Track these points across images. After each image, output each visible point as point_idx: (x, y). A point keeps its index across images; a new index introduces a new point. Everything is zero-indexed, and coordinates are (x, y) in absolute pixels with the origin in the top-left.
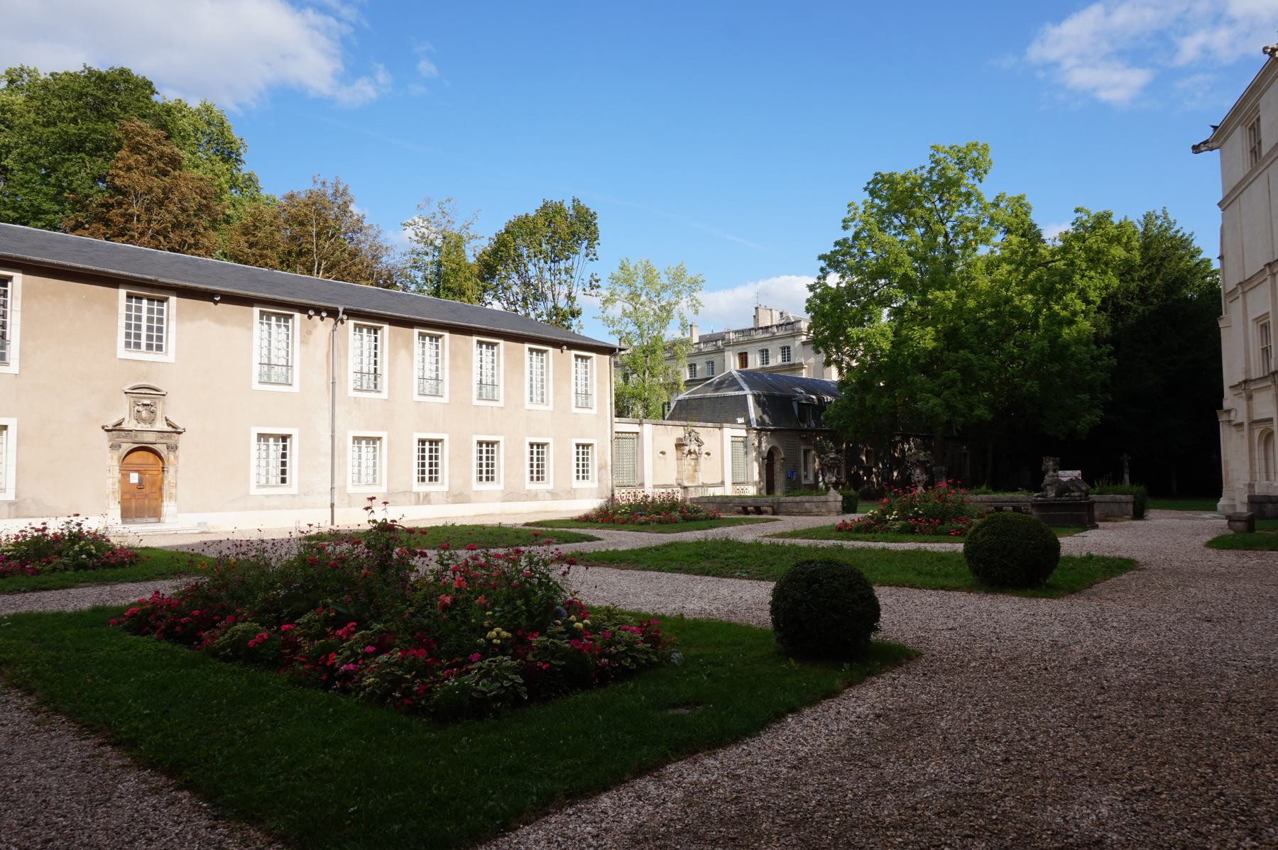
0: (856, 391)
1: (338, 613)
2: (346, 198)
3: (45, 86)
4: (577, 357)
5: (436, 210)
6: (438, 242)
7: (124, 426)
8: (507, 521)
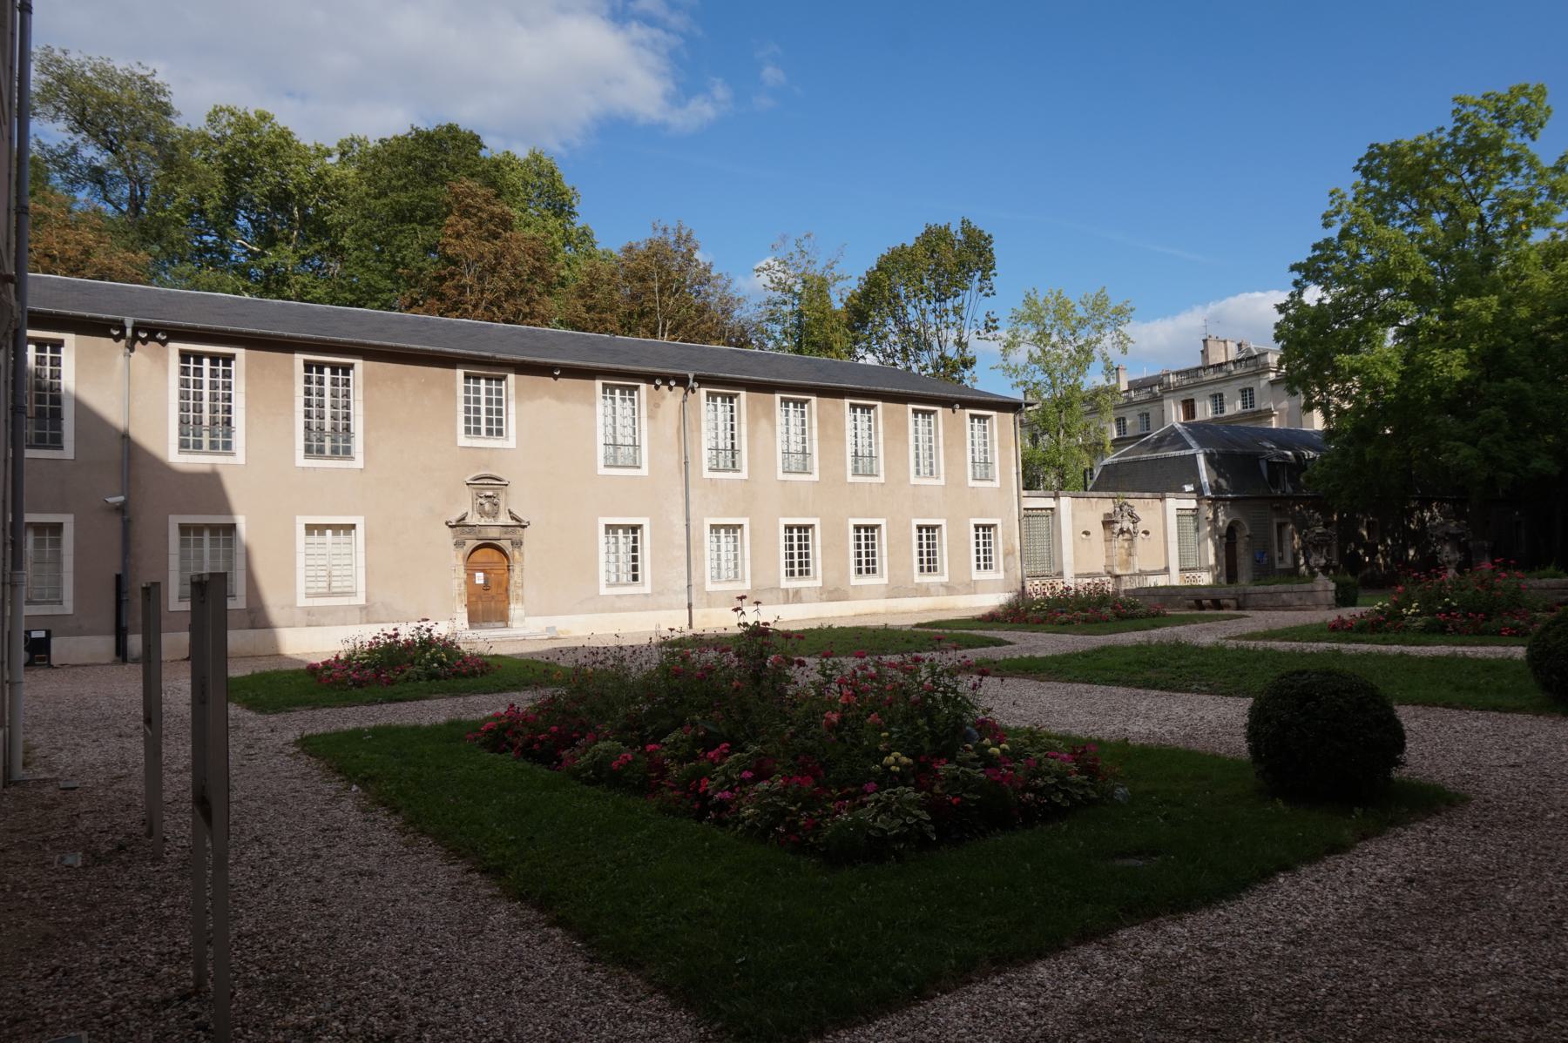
0: (1350, 442)
1: (708, 732)
2: (691, 245)
3: (375, 155)
4: (972, 417)
5: (794, 249)
6: (798, 288)
7: (468, 521)
8: (895, 622)
